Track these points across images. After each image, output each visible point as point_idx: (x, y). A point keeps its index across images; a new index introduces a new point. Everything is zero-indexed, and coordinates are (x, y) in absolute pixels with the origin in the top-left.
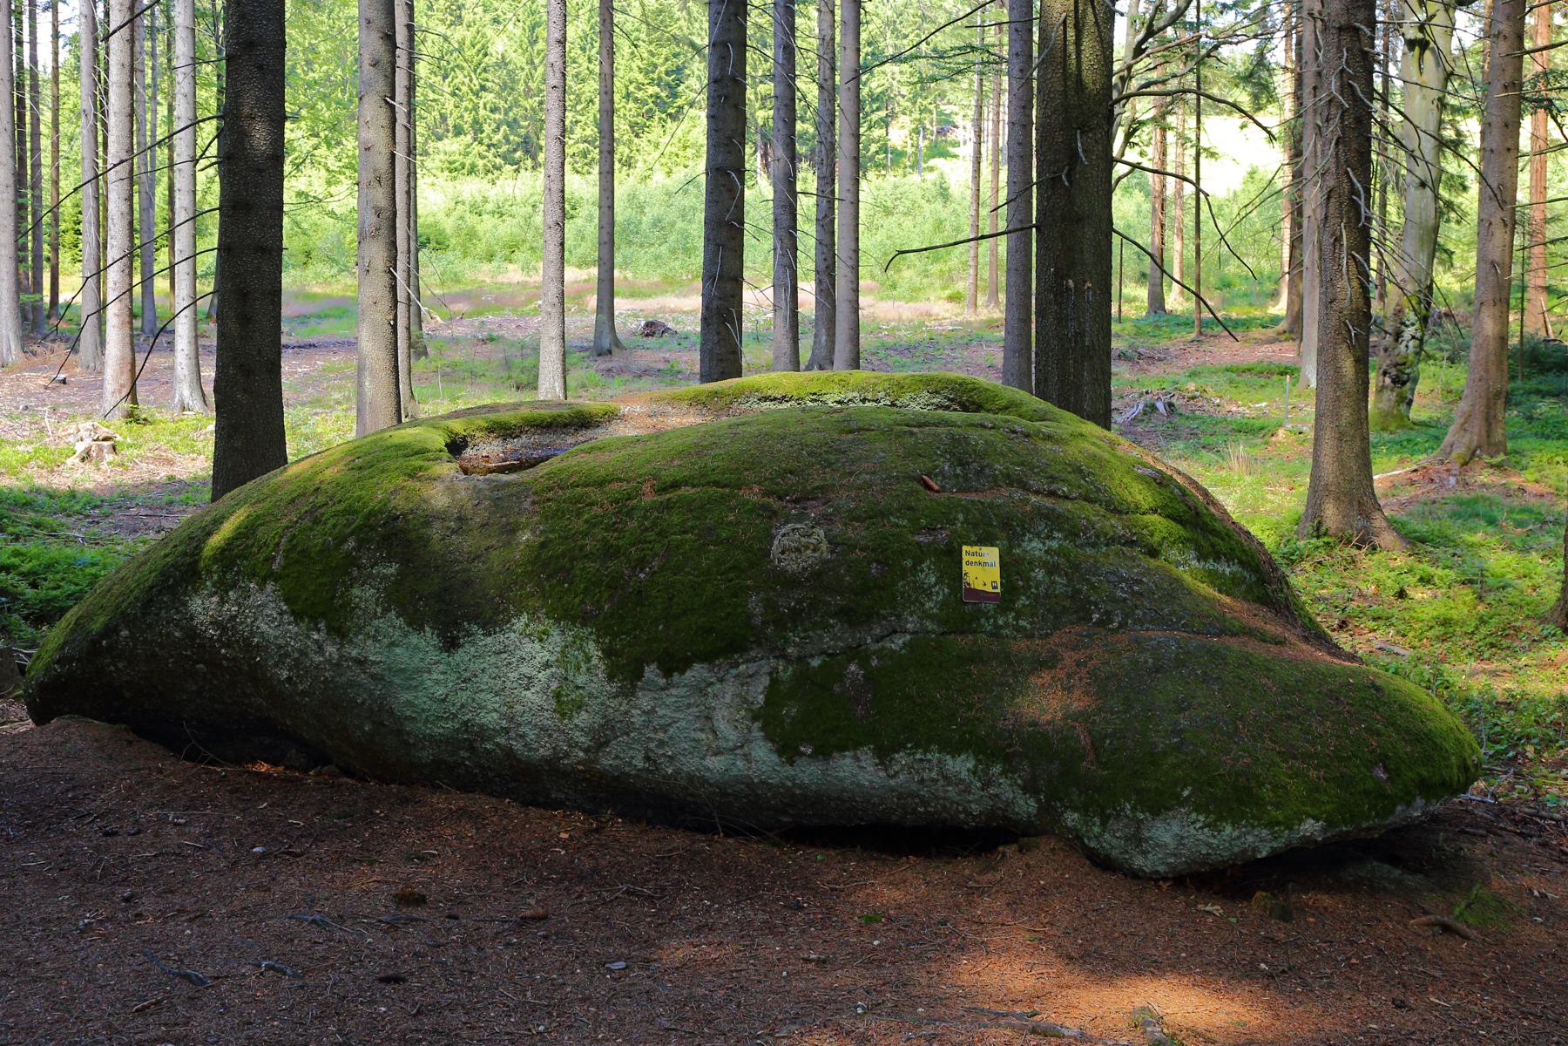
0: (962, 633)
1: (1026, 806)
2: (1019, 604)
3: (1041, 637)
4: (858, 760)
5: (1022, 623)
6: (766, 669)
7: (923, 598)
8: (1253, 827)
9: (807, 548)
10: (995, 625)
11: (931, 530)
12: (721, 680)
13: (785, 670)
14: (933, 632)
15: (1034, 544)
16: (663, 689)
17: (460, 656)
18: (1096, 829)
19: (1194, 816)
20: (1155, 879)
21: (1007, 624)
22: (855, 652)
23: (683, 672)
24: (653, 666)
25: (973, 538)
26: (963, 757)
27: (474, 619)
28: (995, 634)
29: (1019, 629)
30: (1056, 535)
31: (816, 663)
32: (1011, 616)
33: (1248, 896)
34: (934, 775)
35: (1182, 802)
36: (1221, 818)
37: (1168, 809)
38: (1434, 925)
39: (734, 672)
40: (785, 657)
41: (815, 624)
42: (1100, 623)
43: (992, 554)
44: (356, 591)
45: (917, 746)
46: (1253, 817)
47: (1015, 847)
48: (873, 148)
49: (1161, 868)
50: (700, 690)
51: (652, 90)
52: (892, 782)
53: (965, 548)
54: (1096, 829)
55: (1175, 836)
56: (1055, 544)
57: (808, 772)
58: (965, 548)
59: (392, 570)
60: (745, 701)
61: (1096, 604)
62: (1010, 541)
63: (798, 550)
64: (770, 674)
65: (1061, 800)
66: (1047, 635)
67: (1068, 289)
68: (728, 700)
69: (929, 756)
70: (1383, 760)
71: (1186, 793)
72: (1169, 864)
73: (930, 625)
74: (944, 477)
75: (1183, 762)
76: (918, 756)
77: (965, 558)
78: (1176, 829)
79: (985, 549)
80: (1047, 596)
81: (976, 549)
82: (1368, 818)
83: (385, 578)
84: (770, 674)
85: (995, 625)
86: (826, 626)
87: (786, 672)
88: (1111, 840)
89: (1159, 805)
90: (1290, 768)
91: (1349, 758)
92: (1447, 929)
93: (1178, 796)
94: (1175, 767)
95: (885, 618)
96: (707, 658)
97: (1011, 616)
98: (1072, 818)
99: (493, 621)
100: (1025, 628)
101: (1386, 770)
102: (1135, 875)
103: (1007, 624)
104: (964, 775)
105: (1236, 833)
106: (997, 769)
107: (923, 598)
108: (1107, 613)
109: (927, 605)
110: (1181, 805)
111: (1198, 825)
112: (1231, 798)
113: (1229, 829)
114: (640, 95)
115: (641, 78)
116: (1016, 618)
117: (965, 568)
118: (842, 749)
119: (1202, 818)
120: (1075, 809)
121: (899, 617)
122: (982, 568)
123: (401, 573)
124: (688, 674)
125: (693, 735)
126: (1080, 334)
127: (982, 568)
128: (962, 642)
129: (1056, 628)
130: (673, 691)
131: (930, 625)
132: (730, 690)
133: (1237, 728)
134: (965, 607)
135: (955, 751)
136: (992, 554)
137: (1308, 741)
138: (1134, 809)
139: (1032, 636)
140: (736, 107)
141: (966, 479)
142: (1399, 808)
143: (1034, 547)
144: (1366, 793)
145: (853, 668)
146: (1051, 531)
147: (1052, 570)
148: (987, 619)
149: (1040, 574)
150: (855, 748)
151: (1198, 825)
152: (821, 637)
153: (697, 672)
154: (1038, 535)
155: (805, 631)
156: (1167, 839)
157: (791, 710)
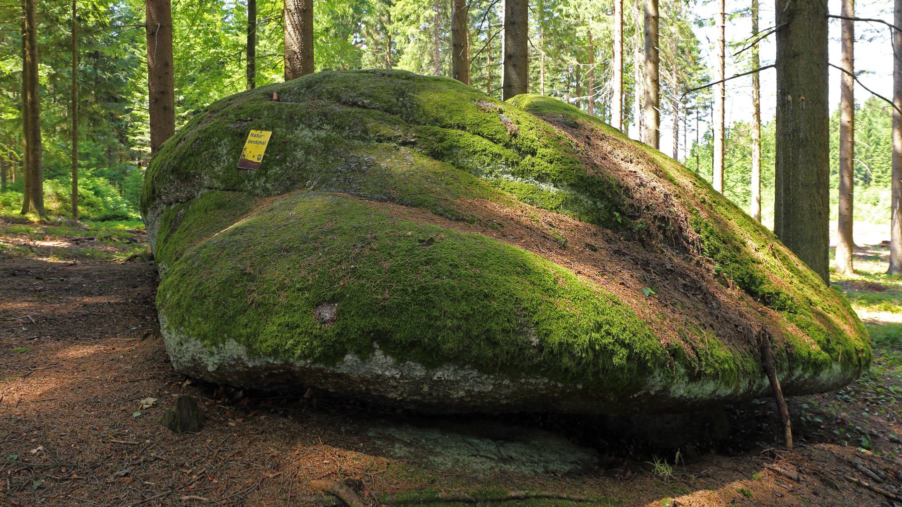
0: (234, 190)
7: (214, 164)
15: (305, 132)
30: (326, 127)
53: (252, 131)
56: (323, 134)
58: (252, 131)
77: (250, 138)
81: (259, 132)
97: (263, 179)
107: (214, 164)
117: (247, 145)
126: (796, 130)
142: (348, 357)
149: (300, 154)
154: (310, 126)
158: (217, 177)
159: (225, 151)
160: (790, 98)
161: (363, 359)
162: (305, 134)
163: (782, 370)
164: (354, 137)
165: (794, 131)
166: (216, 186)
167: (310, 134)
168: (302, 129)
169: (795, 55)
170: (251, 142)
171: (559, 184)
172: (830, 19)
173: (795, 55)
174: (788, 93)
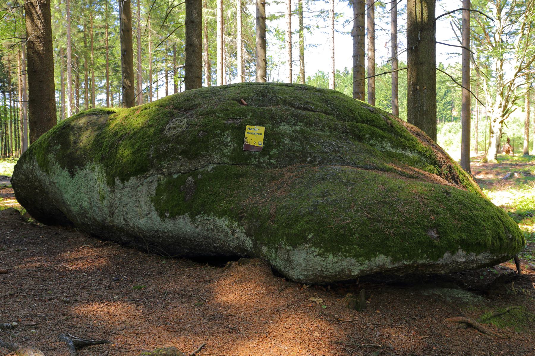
0: (242, 165)
1: (249, 244)
2: (272, 153)
3: (281, 168)
4: (185, 220)
5: (272, 161)
6: (156, 179)
7: (223, 148)
8: (346, 257)
9: (178, 127)
10: (259, 162)
11: (233, 119)
12: (142, 184)
13: (164, 179)
14: (228, 163)
15: (286, 127)
16: (123, 189)
17: (76, 179)
18: (274, 255)
19: (313, 249)
20: (298, 283)
21: (264, 162)
22: (193, 172)
23: (128, 181)
24: (118, 178)
25: (254, 123)
26: (223, 218)
27: (77, 164)
28: (259, 166)
29: (270, 164)
30: (299, 124)
31: (175, 176)
32: (267, 158)
33: (342, 296)
34: (212, 227)
35: (307, 241)
36: (327, 250)
37: (300, 245)
38: (460, 322)
39: (146, 180)
40: (163, 173)
41: (172, 158)
42: (311, 162)
43: (261, 130)
44: (49, 156)
45: (205, 213)
46: (346, 251)
47: (237, 262)
48: (448, 116)
49: (301, 277)
50: (135, 188)
51: (385, 102)
52: (197, 230)
53: (247, 126)
54: (274, 255)
55: (305, 260)
56: (298, 128)
57: (169, 226)
58: (247, 126)
59: (58, 147)
60: (150, 194)
61: (310, 153)
62: (273, 125)
63: (175, 128)
64: (158, 181)
65: (259, 240)
66: (283, 167)
67: (417, 89)
68: (144, 193)
69: (210, 218)
70: (437, 226)
71: (310, 236)
72: (304, 275)
73: (226, 160)
74: (252, 101)
75: (312, 220)
76: (205, 218)
77: (247, 131)
78: (304, 255)
79: (257, 127)
80: (289, 150)
81: (253, 127)
82: (422, 258)
83: (57, 150)
84: (158, 181)
85: (259, 162)
86: (178, 159)
87: (164, 180)
88: (279, 262)
89: (296, 241)
90: (374, 226)
91: (413, 224)
92: (469, 326)
93: (306, 238)
94: (307, 222)
95: (204, 156)
96: (135, 174)
97: (267, 158)
98: (265, 249)
99: (81, 165)
100: (273, 164)
101: (438, 232)
102: (289, 280)
103: (264, 162)
104: (224, 227)
105: (335, 259)
106: (235, 224)
107: (223, 148)
108: (315, 157)
109: (225, 151)
110: (306, 242)
111: (315, 254)
112: (334, 241)
113: (331, 257)
114: (383, 104)
115: (383, 99)
116: (269, 159)
117: (246, 135)
118: (179, 214)
119: (317, 250)
120: (266, 245)
121: (210, 155)
122: (255, 136)
123: (61, 148)
124: (130, 181)
125: (135, 209)
126: (422, 106)
127: (255, 136)
128: (240, 169)
129: (289, 164)
130: (126, 189)
131: (226, 160)
132: (145, 188)
133: (350, 205)
134: (243, 154)
135: (221, 216)
136: (261, 130)
137: (390, 214)
138: (285, 245)
139: (277, 167)
140: (361, 74)
141: (263, 101)
142: (446, 255)
143: (286, 128)
144: (420, 243)
145: (190, 179)
146: (297, 122)
147: (293, 139)
148: (255, 158)
149: (287, 141)
150: (184, 214)
151: (315, 254)
152: (176, 165)
153: (132, 181)
154: (289, 123)
155: (168, 161)
156: (301, 261)
157: (164, 197)
158: (225, 156)
159: (229, 139)
160: (418, 87)
161: (453, 255)
162: (286, 128)
163: (167, 209)
164: (317, 130)
165: (420, 106)
166: (226, 162)
167: (290, 128)
168: (284, 125)
169: (421, 64)
170: (248, 133)
171: (413, 152)
172: (437, 44)
173: (421, 64)
174: (417, 85)
